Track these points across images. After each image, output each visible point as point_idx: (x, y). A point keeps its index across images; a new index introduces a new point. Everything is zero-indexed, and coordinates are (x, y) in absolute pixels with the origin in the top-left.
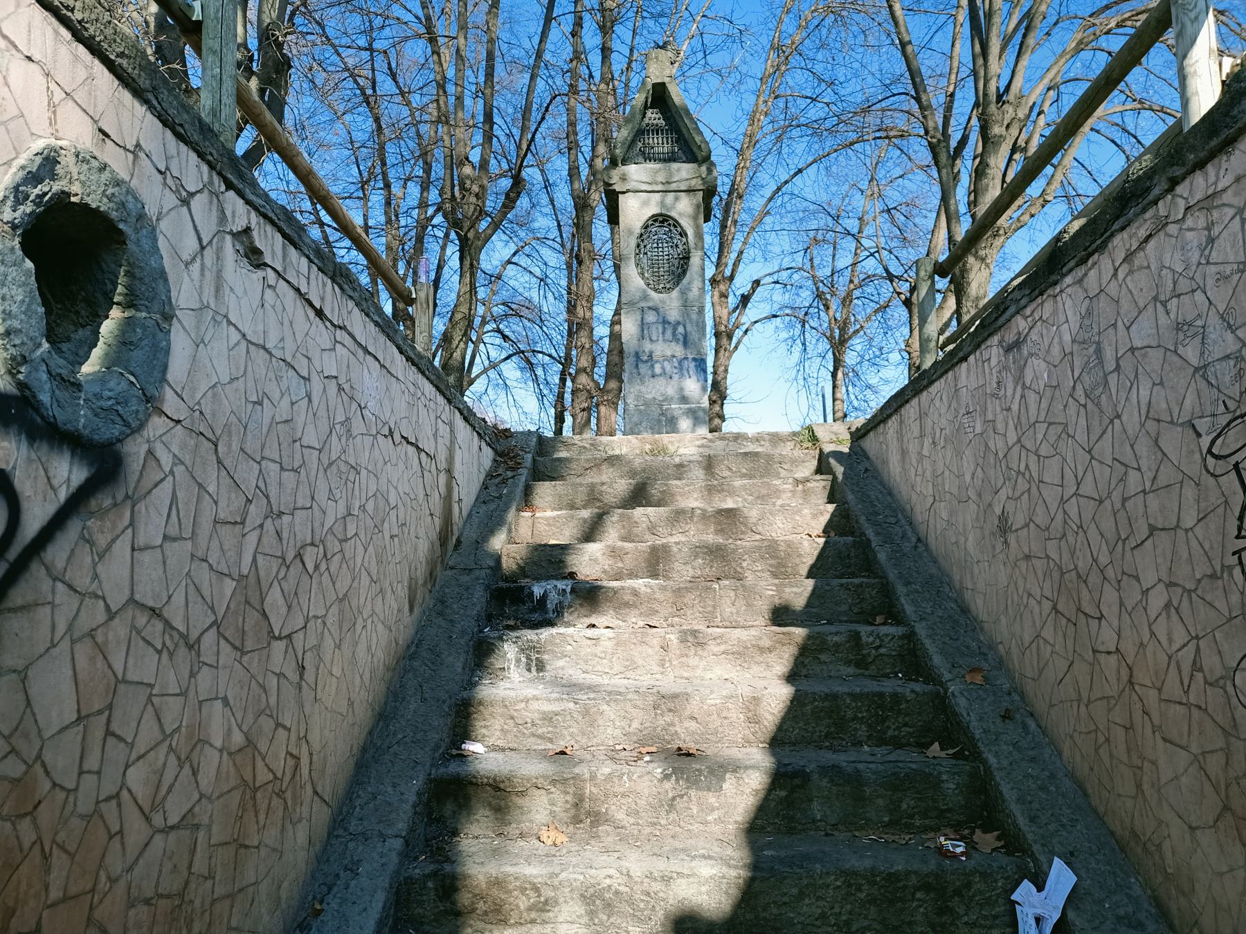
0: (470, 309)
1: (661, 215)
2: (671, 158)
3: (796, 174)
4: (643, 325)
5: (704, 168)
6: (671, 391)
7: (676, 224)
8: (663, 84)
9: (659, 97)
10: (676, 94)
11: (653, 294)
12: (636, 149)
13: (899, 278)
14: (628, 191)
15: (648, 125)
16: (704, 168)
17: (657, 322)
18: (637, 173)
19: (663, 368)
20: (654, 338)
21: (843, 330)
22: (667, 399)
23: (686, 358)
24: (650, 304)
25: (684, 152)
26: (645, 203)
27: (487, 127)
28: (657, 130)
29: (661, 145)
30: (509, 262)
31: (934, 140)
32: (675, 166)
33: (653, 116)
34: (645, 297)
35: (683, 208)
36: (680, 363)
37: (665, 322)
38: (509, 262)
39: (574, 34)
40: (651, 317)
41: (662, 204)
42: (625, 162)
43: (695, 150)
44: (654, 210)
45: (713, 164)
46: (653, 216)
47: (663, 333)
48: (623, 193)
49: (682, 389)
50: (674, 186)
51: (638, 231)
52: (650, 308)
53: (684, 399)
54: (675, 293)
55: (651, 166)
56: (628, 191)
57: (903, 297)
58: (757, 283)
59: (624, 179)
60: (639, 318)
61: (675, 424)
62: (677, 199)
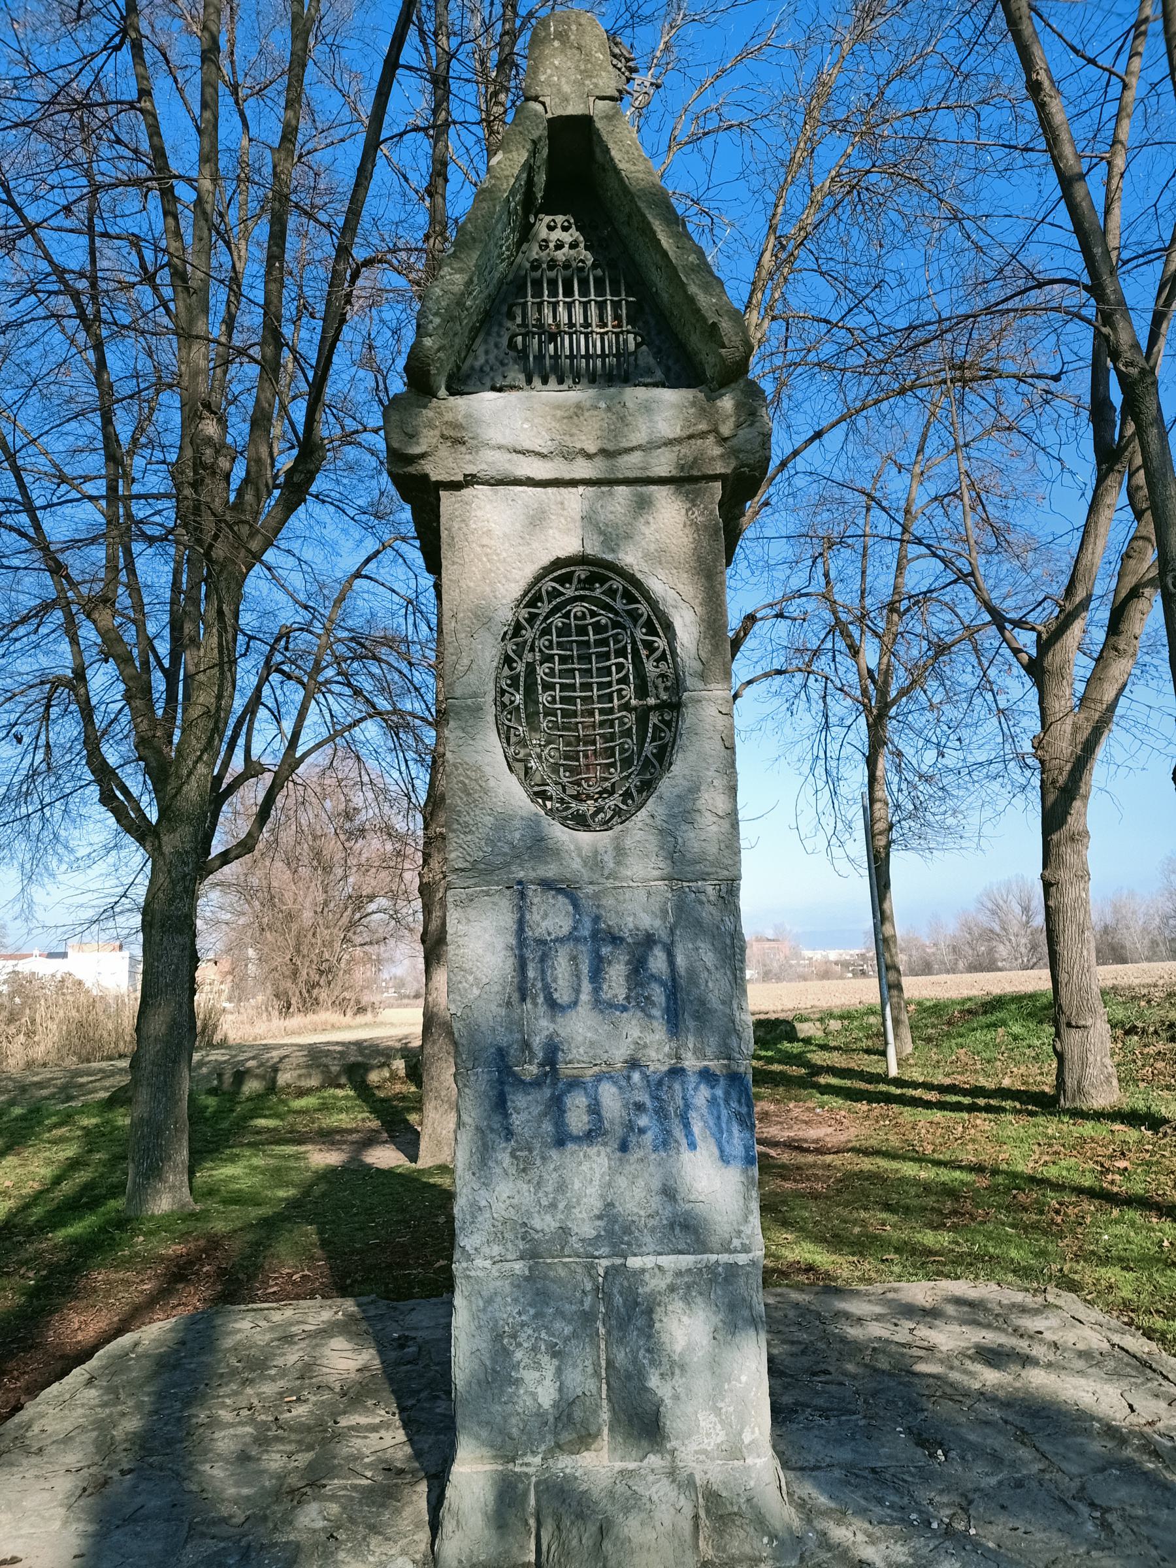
0: (219, 697)
1: (581, 560)
2: (615, 374)
3: (811, 440)
4: (528, 950)
5: (727, 403)
6: (637, 1197)
7: (634, 589)
8: (585, 121)
9: (573, 167)
10: (630, 151)
11: (558, 832)
12: (493, 338)
13: (1019, 624)
14: (470, 480)
15: (536, 265)
16: (727, 403)
17: (572, 937)
18: (510, 420)
19: (595, 1109)
20: (563, 995)
21: (883, 692)
22: (617, 1232)
23: (676, 1072)
24: (550, 871)
25: (657, 353)
26: (537, 520)
27: (269, 351)
28: (571, 278)
29: (586, 322)
30: (358, 575)
31: (1134, 371)
32: (635, 395)
33: (558, 236)
34: (538, 846)
35: (660, 541)
36: (656, 1086)
37: (603, 938)
38: (358, 575)
39: (431, 192)
40: (551, 918)
41: (589, 520)
42: (460, 385)
43: (695, 341)
44: (565, 542)
45: (754, 392)
46: (557, 563)
47: (597, 975)
48: (455, 486)
49: (669, 1193)
50: (630, 464)
51: (505, 614)
52: (547, 885)
53: (686, 1229)
54: (639, 830)
55: (552, 396)
56: (470, 480)
57: (1025, 658)
58: (751, 619)
59: (457, 441)
60: (508, 919)
61: (648, 1331)
62: (643, 505)
